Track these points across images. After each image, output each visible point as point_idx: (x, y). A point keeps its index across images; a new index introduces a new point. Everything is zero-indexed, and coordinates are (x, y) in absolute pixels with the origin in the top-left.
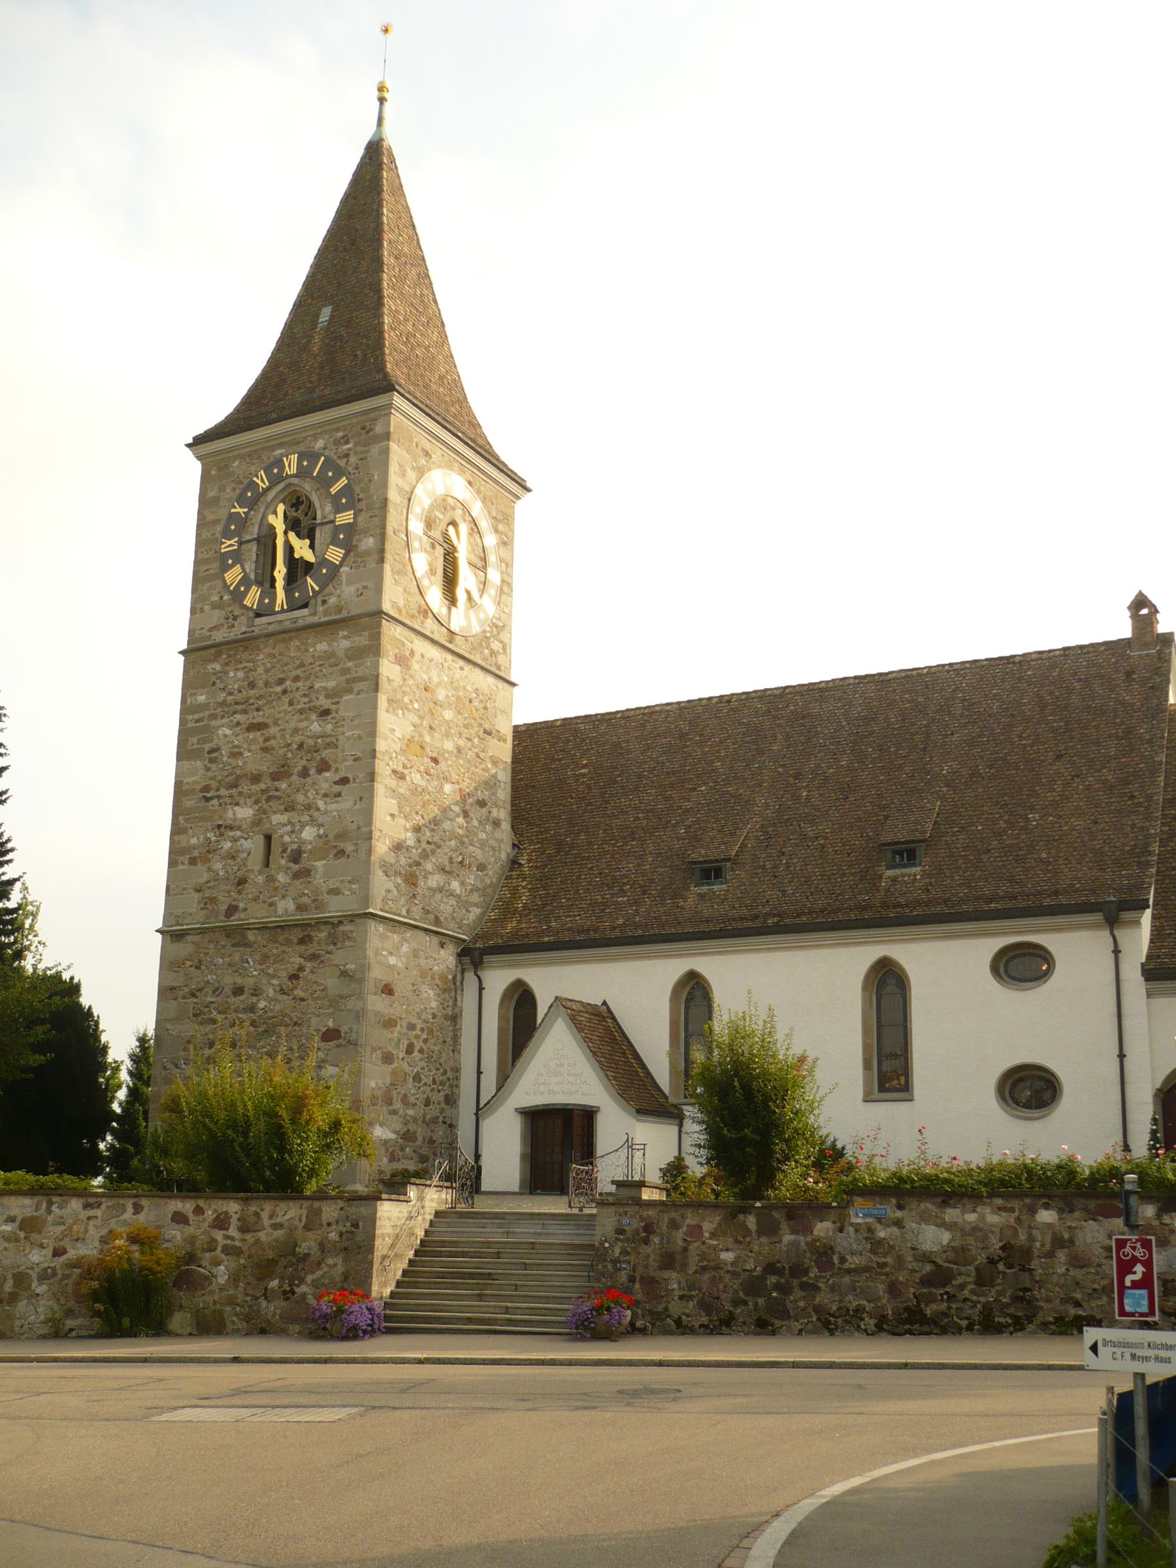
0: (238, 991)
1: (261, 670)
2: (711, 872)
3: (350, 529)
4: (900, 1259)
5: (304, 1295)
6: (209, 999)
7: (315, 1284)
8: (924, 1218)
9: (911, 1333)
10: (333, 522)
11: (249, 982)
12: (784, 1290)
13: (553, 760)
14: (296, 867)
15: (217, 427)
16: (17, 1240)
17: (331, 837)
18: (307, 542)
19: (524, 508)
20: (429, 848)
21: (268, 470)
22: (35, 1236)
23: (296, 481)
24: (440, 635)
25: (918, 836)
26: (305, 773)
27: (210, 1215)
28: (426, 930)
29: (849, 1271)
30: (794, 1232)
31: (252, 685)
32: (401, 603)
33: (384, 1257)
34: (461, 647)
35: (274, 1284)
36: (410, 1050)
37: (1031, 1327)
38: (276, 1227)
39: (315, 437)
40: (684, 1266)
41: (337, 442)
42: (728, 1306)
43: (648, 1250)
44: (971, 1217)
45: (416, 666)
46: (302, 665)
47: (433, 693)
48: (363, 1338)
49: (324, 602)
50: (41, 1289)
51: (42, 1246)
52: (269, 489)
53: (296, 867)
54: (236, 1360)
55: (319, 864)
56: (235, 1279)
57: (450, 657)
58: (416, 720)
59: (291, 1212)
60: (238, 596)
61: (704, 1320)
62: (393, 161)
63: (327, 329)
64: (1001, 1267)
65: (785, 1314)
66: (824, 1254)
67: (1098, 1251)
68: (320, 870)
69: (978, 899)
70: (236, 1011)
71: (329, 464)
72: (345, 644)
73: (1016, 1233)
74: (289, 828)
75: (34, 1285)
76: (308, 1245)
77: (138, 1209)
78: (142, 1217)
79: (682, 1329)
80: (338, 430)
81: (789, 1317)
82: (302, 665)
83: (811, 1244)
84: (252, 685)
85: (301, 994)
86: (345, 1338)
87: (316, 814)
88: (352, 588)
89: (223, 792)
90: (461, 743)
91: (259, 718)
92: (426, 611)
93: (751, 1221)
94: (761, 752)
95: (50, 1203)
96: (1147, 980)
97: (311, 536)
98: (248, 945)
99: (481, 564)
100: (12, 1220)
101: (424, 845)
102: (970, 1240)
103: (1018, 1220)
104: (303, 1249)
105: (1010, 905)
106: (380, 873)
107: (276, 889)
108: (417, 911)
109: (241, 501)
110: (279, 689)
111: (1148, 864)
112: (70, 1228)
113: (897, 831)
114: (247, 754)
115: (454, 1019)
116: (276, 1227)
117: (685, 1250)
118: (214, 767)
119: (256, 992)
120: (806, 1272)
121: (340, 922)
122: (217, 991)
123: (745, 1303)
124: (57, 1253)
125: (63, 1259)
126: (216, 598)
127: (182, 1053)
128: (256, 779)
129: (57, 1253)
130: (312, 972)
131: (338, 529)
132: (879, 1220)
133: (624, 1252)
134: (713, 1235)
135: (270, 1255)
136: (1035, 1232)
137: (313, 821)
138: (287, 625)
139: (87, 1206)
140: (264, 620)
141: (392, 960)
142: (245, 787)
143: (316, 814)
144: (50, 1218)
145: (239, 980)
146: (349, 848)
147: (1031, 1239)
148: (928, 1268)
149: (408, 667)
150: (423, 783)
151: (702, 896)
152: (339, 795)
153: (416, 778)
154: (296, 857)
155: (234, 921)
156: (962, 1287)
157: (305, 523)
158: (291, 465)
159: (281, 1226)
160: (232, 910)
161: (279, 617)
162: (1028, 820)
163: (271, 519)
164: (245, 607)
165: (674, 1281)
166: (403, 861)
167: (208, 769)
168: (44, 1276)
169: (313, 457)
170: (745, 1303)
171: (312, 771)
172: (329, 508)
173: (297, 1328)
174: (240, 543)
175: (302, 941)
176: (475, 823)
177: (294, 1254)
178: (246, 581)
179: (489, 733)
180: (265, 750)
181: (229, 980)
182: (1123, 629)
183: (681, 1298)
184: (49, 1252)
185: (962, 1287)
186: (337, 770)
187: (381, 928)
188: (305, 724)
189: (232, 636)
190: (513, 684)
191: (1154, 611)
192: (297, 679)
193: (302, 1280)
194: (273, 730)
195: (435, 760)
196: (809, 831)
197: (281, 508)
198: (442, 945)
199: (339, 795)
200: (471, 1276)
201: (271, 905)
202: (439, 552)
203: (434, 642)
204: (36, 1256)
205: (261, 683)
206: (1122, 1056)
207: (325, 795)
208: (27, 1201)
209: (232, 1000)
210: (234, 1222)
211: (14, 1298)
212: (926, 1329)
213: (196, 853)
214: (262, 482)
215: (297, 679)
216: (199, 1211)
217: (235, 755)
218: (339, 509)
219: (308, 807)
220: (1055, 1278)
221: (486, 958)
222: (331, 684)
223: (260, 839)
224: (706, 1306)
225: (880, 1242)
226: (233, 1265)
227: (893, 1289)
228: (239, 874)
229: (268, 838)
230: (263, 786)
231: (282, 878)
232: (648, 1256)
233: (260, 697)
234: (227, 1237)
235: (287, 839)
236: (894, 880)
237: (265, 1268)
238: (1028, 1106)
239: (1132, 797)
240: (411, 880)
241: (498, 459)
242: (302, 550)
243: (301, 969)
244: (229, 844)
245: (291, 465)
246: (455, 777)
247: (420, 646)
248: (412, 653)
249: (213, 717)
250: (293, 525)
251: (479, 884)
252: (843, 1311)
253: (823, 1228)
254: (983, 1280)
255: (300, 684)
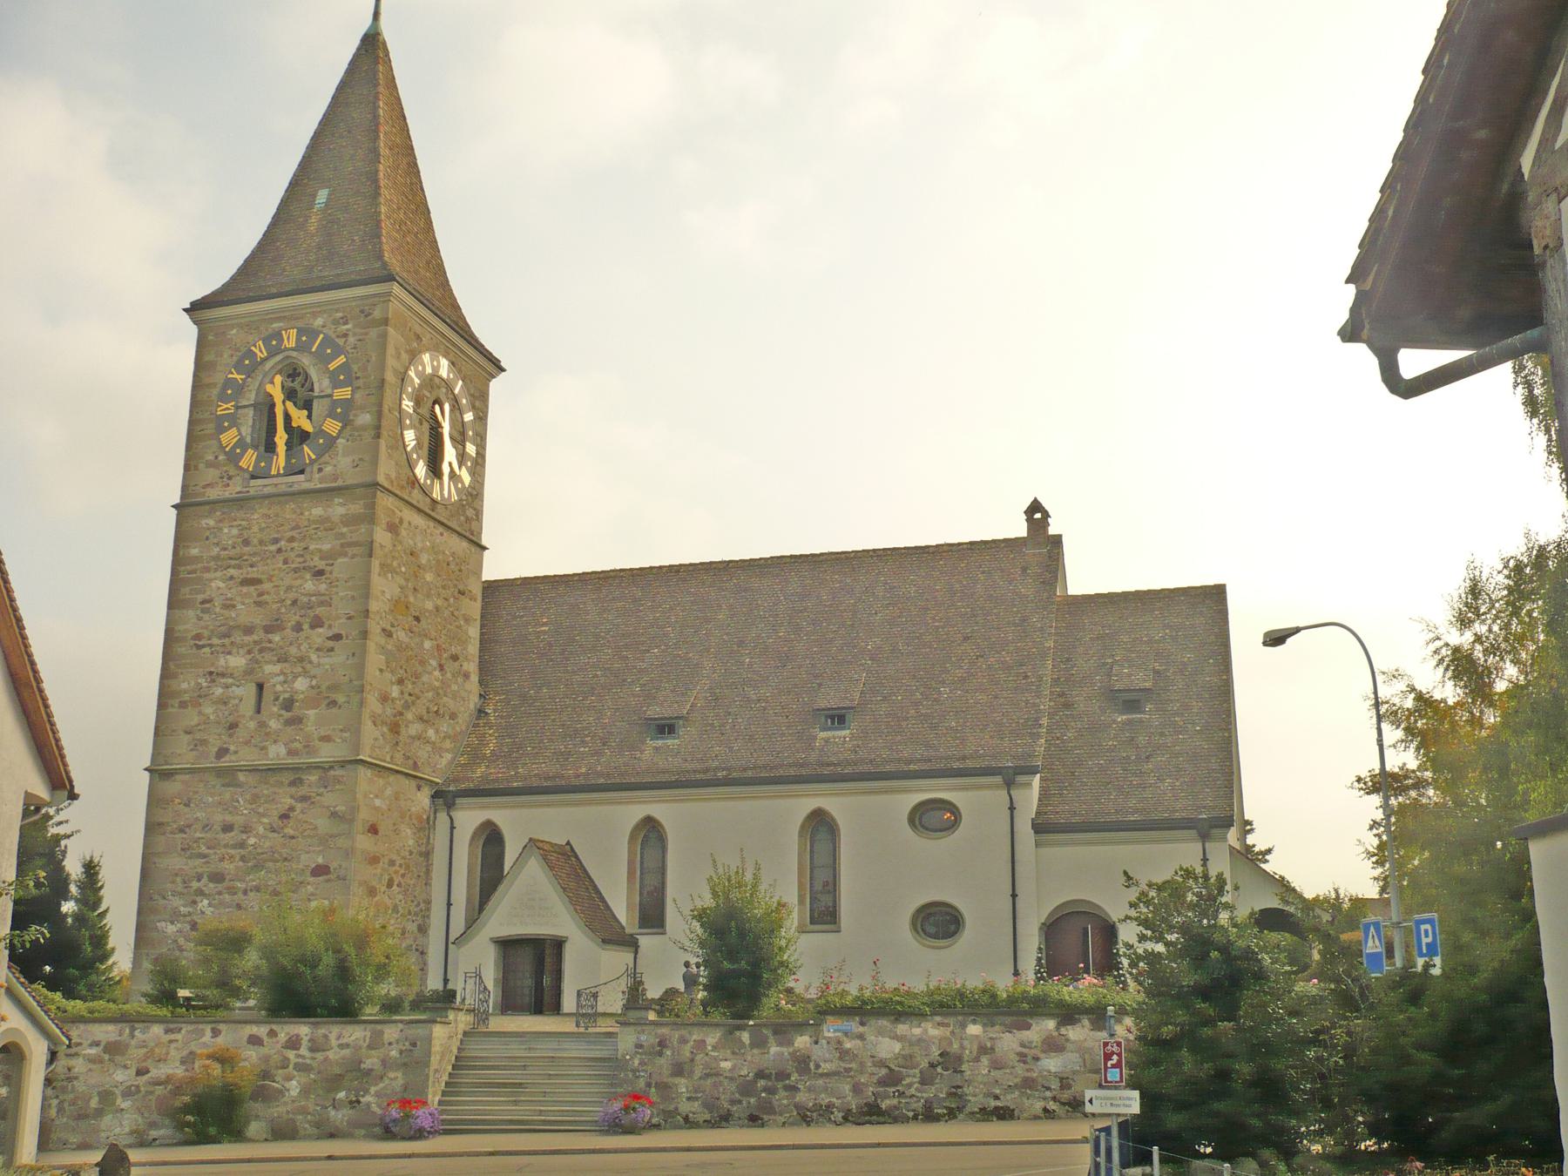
0: (228, 828)
1: (255, 528)
2: (666, 728)
3: (348, 404)
4: (862, 1064)
5: (368, 1105)
6: (198, 835)
7: (378, 1095)
8: (881, 1033)
9: (870, 1123)
10: (330, 396)
11: (239, 820)
12: (771, 1091)
13: (515, 617)
14: (287, 715)
15: (214, 294)
16: (101, 1061)
17: (323, 688)
18: (305, 412)
19: (496, 386)
20: (410, 699)
21: (266, 341)
22: (118, 1058)
23: (294, 354)
24: (424, 504)
25: (847, 703)
26: (298, 628)
27: (282, 1037)
28: (407, 775)
29: (822, 1075)
30: (780, 1044)
31: (246, 542)
32: (393, 475)
33: (436, 1071)
34: (441, 514)
35: (342, 1095)
36: (390, 885)
37: (961, 1116)
38: (341, 1046)
39: (315, 315)
40: (692, 1072)
41: (336, 322)
42: (726, 1105)
43: (662, 1061)
44: (917, 1031)
45: (404, 533)
46: (297, 527)
47: (417, 557)
48: (426, 1138)
49: (320, 470)
50: (125, 1105)
51: (125, 1067)
52: (266, 359)
53: (287, 715)
54: (330, 1158)
55: (311, 713)
56: (305, 1091)
57: (432, 524)
58: (403, 582)
59: (355, 1034)
60: (233, 458)
61: (707, 1116)
62: (387, 54)
63: (324, 211)
64: (939, 1069)
65: (770, 1110)
66: (803, 1062)
67: (1013, 1056)
68: (312, 718)
69: (899, 760)
70: (226, 846)
71: (328, 341)
72: (341, 510)
73: (951, 1044)
74: (281, 678)
75: (119, 1101)
76: (371, 1061)
77: (216, 1033)
78: (220, 1040)
79: (689, 1123)
80: (337, 311)
81: (775, 1113)
82: (297, 527)
83: (792, 1054)
84: (246, 542)
85: (292, 832)
86: (411, 1138)
87: (309, 666)
88: (348, 460)
89: (215, 641)
90: (439, 602)
91: (253, 573)
92: (414, 481)
93: (745, 1037)
94: (708, 621)
95: (133, 1030)
96: (1036, 832)
97: (307, 406)
98: (239, 785)
99: (459, 441)
100: (97, 1044)
101: (406, 696)
102: (916, 1049)
103: (953, 1033)
104: (366, 1066)
105: (925, 767)
106: (369, 723)
107: (267, 734)
108: (399, 757)
109: (239, 367)
110: (273, 548)
111: (1039, 736)
112: (152, 1050)
113: (829, 699)
114: (239, 606)
115: (427, 855)
116: (341, 1046)
117: (692, 1060)
118: (206, 617)
119: (246, 829)
120: (788, 1076)
121: (331, 768)
122: (206, 827)
123: (740, 1102)
124: (139, 1073)
125: (146, 1077)
126: (210, 457)
127: (169, 886)
128: (249, 630)
129: (139, 1073)
130: (302, 812)
131: (335, 404)
132: (846, 1034)
133: (642, 1063)
134: (715, 1048)
135: (338, 1071)
136: (966, 1043)
137: (305, 673)
138: (283, 488)
139: (167, 1031)
140: (259, 482)
141: (378, 802)
142: (238, 637)
143: (309, 666)
144: (133, 1042)
145: (229, 818)
146: (341, 699)
147: (962, 1047)
148: (884, 1071)
149: (397, 534)
150: (407, 640)
151: (656, 749)
152: (332, 649)
153: (401, 635)
154: (288, 705)
155: (226, 762)
156: (910, 1086)
157: (302, 394)
158: (290, 339)
159: (348, 1046)
160: (222, 752)
161: (275, 481)
162: (940, 693)
163: (269, 388)
164: (241, 468)
165: (682, 1085)
166: (389, 711)
167: (200, 619)
168: (128, 1093)
169: (313, 334)
170: (740, 1102)
171: (306, 626)
172: (326, 382)
173: (363, 1132)
174: (237, 408)
175: (292, 783)
176: (449, 675)
177: (359, 1070)
178: (241, 444)
179: (462, 593)
180: (258, 604)
181: (219, 818)
182: (1019, 529)
183: (689, 1099)
184: (133, 1071)
185: (910, 1086)
186: (330, 626)
187: (369, 773)
188: (299, 582)
189: (227, 495)
190: (485, 548)
191: (1046, 515)
192: (292, 539)
193: (367, 1092)
194: (267, 586)
195: (417, 619)
196: (752, 695)
197: (278, 379)
198: (419, 788)
199: (332, 649)
200: (505, 1085)
201: (263, 748)
202: (426, 426)
203: (419, 510)
204: (120, 1076)
205: (255, 541)
206: (1014, 896)
207: (318, 649)
208: (111, 1027)
209: (222, 836)
210: (305, 1042)
211: (99, 1113)
212: (881, 1119)
213: (186, 697)
214: (260, 351)
215: (292, 539)
216: (272, 1034)
217: (229, 606)
218: (336, 384)
219: (301, 659)
220: (980, 1079)
221: (458, 801)
222: (326, 547)
223: (253, 688)
224: (708, 1106)
225: (847, 1052)
226: (304, 1080)
227: (857, 1089)
228: (231, 719)
229: (260, 687)
230: (255, 637)
231: (273, 724)
232: (661, 1067)
233: (255, 554)
234: (298, 1056)
235: (279, 688)
236: (827, 741)
237: (334, 1082)
238: (936, 936)
239: (1026, 677)
240: (395, 729)
241: (476, 340)
242: (300, 419)
243: (292, 809)
244: (220, 690)
245: (290, 339)
246: (434, 634)
247: (408, 515)
248: (401, 521)
249: (207, 569)
250: (290, 395)
251: (451, 732)
252: (817, 1108)
253: (802, 1041)
254: (925, 1081)
255: (295, 544)
